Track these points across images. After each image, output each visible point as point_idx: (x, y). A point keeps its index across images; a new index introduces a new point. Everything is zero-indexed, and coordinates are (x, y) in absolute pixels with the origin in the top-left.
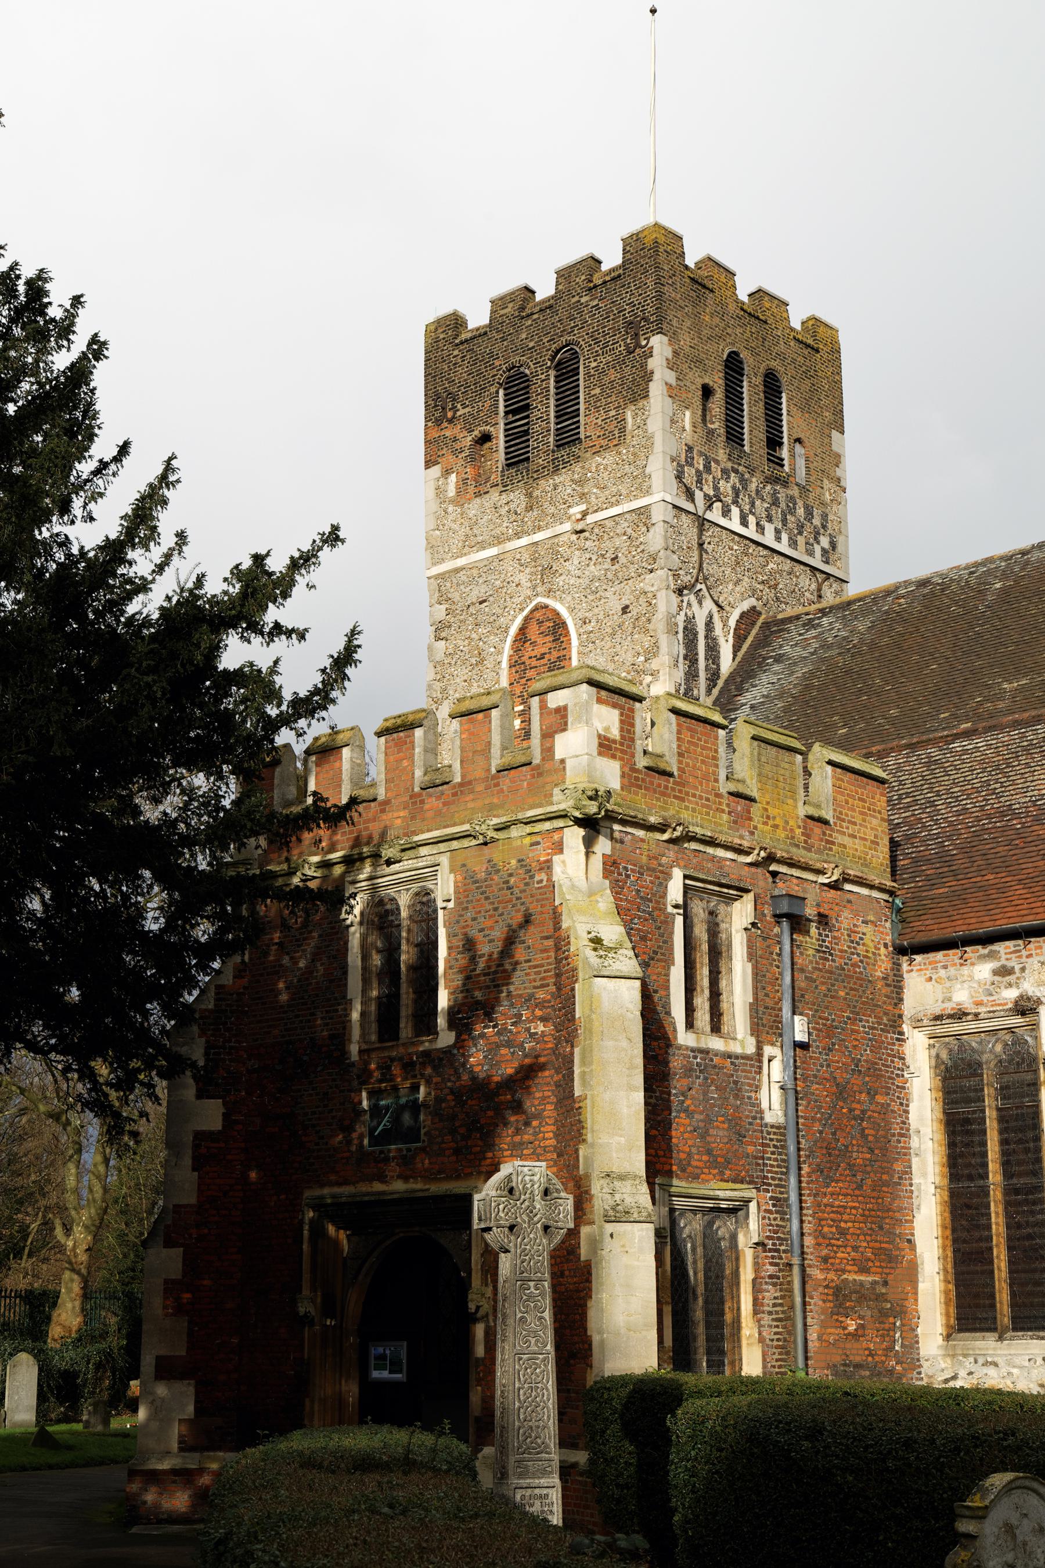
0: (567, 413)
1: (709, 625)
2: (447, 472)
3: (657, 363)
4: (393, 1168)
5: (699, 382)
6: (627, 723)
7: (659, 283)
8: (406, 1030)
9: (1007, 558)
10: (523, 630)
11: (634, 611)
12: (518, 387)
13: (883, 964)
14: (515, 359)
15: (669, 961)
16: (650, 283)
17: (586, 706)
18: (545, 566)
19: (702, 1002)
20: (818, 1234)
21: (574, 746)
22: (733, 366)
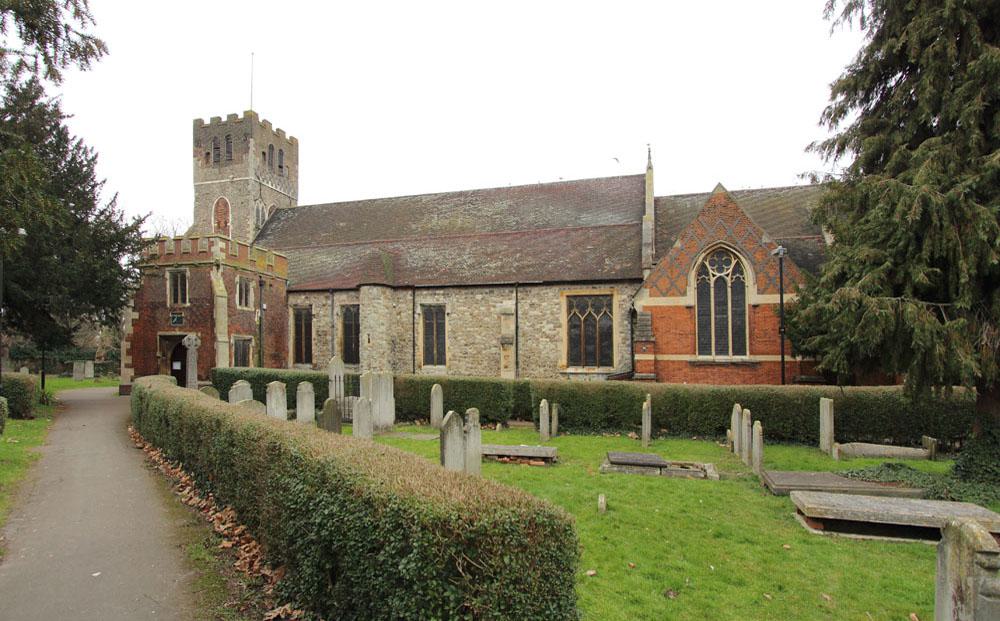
6: (227, 245)
8: (179, 301)
10: (218, 203)
13: (285, 293)
19: (243, 301)
22: (271, 147)
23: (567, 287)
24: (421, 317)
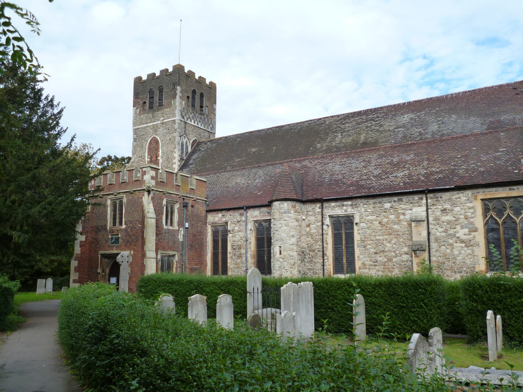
0: (161, 99)
1: (186, 143)
2: (137, 109)
3: (178, 92)
4: (114, 248)
5: (187, 95)
6: (157, 174)
7: (179, 76)
9: (241, 134)
10: (151, 141)
11: (172, 140)
12: (151, 92)
13: (204, 213)
14: (151, 87)
15: (163, 214)
16: (177, 75)
17: (149, 171)
18: (155, 129)
19: (169, 221)
20: (188, 259)
21: (147, 177)
22: (194, 92)
23: (481, 190)
24: (330, 227)
